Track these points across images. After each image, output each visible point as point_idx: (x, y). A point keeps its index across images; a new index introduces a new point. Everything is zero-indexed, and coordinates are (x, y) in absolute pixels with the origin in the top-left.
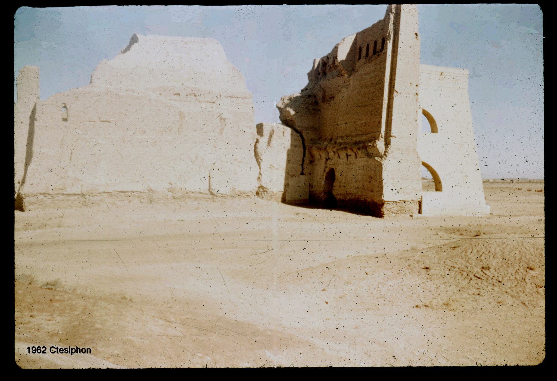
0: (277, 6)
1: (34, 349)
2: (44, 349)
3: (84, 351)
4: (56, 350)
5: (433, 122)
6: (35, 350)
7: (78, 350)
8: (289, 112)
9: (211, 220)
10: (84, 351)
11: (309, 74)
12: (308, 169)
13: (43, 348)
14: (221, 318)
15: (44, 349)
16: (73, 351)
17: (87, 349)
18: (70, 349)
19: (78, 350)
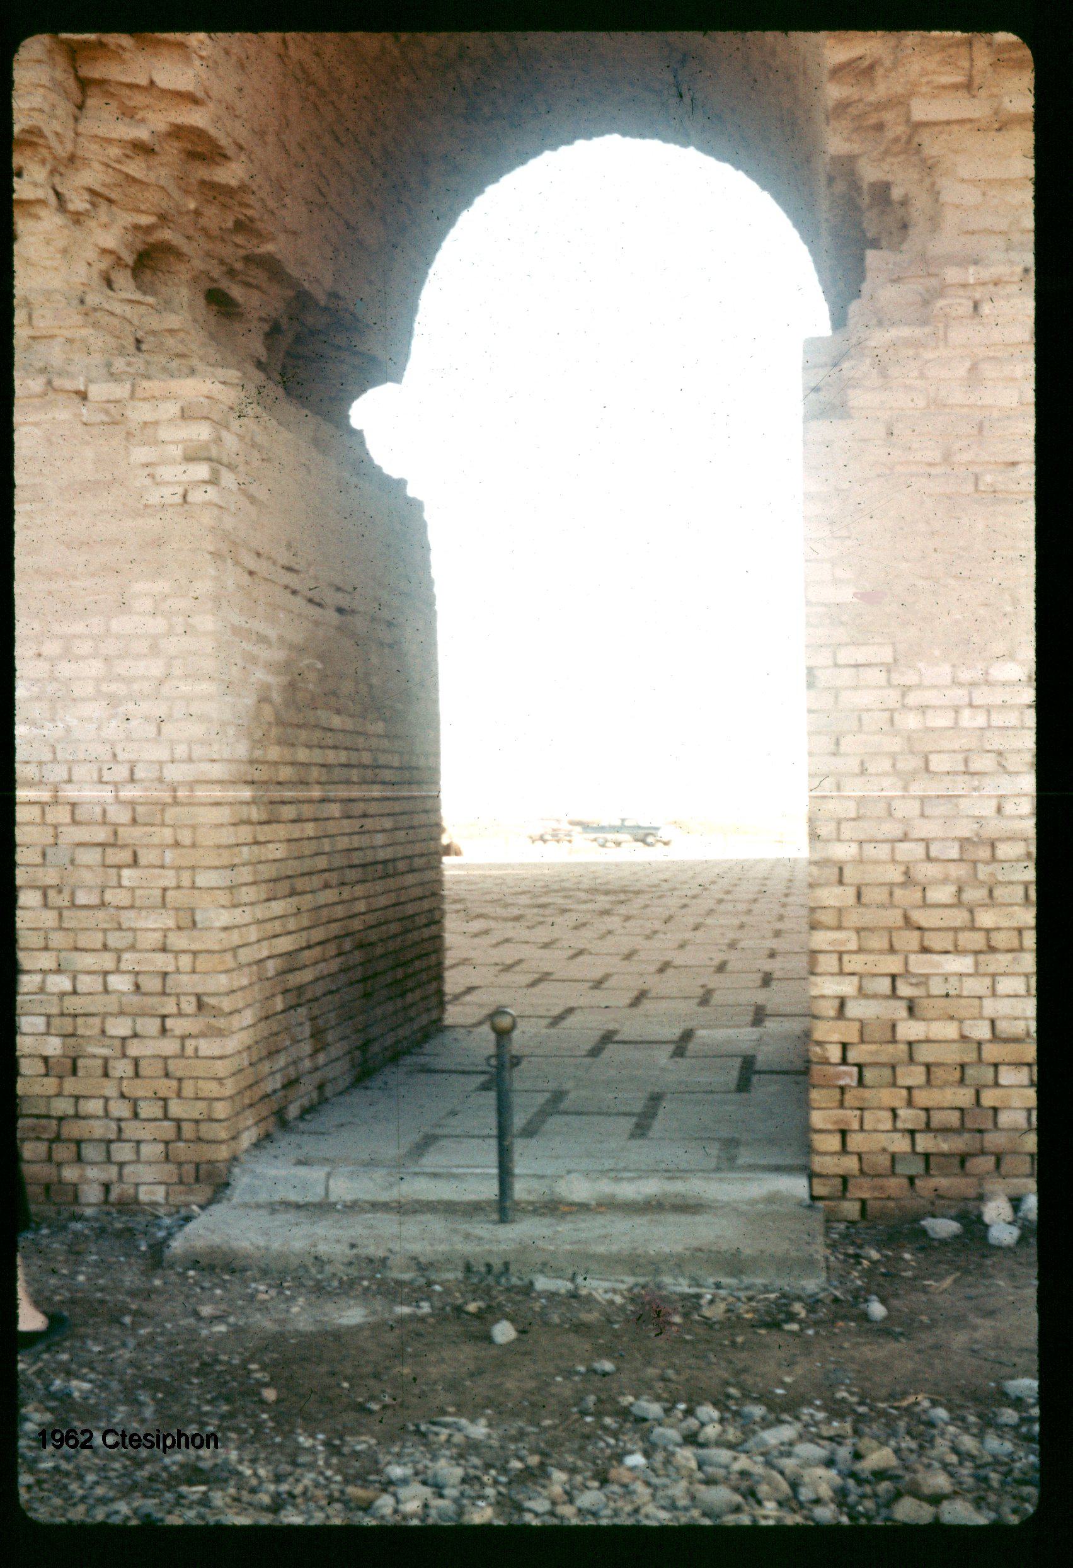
0: (1032, 217)
1: (58, 1436)
2: (87, 1435)
3: (198, 1441)
4: (119, 1439)
5: (731, 1144)
6: (61, 1440)
7: (183, 1440)
8: (144, 1327)
9: (267, 1018)
10: (198, 1441)
11: (397, 378)
12: (213, 191)
13: (83, 1432)
14: (324, 729)
15: (87, 1435)
16: (169, 1442)
17: (208, 1437)
18: (158, 1438)
19: (183, 1440)
